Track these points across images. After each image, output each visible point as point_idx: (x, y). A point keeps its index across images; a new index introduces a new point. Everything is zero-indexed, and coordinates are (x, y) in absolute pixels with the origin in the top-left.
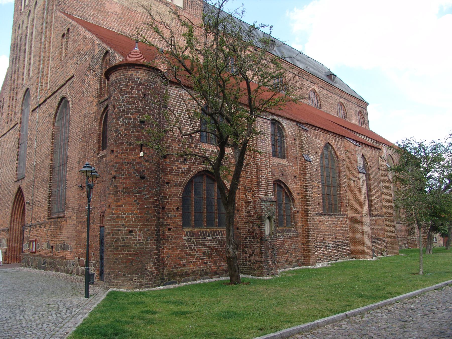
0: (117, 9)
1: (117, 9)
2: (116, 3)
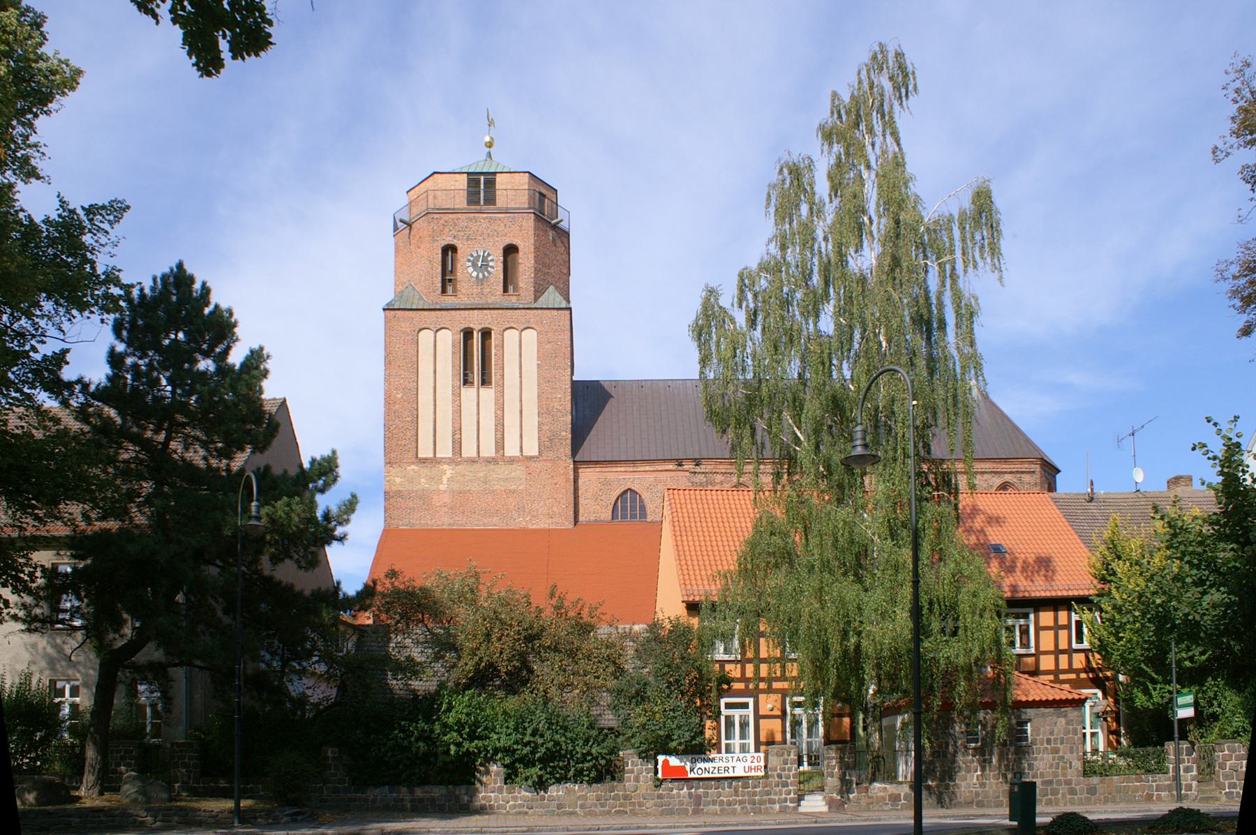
0: (446, 499)
1: (446, 499)
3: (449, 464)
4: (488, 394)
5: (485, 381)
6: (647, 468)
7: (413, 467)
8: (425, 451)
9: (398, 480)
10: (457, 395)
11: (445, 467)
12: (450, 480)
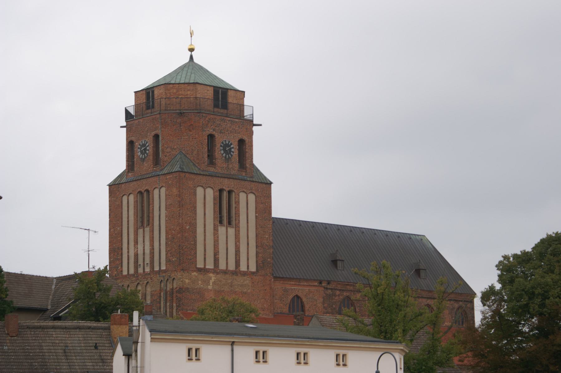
2: (211, 290)
3: (213, 273)
4: (231, 231)
5: (230, 223)
6: (305, 284)
7: (195, 273)
8: (200, 265)
9: (187, 281)
10: (216, 230)
11: (211, 275)
12: (214, 283)
